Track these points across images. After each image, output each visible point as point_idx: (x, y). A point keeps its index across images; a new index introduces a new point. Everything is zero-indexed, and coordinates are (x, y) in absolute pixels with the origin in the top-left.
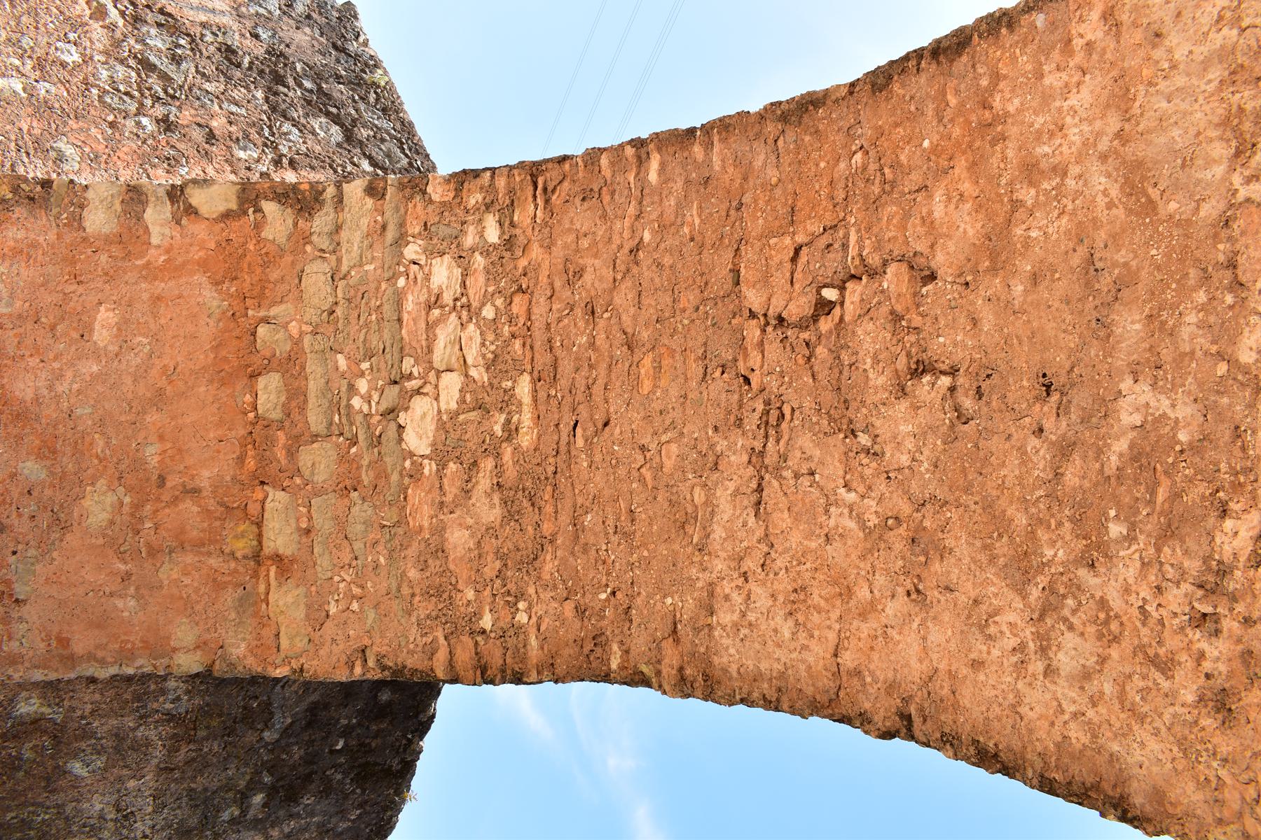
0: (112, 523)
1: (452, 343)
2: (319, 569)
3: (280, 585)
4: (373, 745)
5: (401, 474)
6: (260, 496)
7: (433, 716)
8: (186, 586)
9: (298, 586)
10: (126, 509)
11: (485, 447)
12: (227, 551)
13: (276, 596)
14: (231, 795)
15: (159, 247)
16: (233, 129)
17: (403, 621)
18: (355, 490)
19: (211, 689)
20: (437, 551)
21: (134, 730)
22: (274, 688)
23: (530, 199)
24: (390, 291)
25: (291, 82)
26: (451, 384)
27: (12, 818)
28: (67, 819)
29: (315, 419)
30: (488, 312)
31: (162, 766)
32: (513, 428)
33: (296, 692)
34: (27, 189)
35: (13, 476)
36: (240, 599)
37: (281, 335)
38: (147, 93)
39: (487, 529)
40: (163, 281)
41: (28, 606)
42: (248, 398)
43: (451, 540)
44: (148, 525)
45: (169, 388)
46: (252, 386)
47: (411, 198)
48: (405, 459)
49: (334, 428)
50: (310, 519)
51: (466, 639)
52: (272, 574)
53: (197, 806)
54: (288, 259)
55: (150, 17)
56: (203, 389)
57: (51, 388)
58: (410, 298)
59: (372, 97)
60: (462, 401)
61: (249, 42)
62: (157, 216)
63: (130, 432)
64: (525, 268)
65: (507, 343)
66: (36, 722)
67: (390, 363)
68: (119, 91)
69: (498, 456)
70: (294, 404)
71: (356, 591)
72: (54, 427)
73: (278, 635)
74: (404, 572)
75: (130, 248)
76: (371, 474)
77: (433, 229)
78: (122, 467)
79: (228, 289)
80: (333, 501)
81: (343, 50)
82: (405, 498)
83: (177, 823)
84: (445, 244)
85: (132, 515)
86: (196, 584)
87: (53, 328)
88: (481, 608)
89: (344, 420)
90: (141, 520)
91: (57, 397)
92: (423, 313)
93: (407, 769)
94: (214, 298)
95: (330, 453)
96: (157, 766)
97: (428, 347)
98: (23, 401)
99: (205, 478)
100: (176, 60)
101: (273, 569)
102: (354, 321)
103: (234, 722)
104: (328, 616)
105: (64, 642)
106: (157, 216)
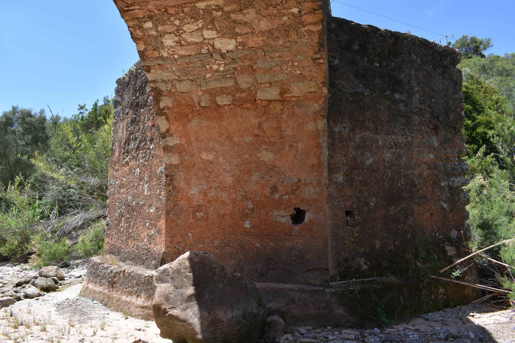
0: (272, 151)
1: (192, 35)
2: (283, 78)
3: (291, 92)
4: (380, 50)
5: (244, 50)
6: (259, 101)
7: (370, 26)
8: (293, 126)
9: (291, 86)
10: (267, 147)
11: (227, 18)
12: (280, 112)
13: (295, 94)
14: (393, 107)
15: (180, 141)
16: (151, 119)
17: (300, 45)
18: (253, 67)
19: (341, 115)
20: (271, 33)
21: (355, 142)
22: (344, 92)
23: (133, 12)
24: (179, 60)
25: (138, 100)
26: (209, 34)
27: (388, 183)
28: (392, 165)
29: (230, 83)
30: (177, 22)
31: (374, 132)
32: (217, 8)
33: (348, 83)
34: (168, 181)
35: (257, 183)
36: (298, 106)
37: (203, 98)
38: (144, 147)
39: (258, 14)
40: (191, 139)
41: (301, 178)
42: (226, 108)
43: (265, 28)
44: (272, 140)
45: (225, 135)
46: (222, 106)
47: (147, 56)
48: (239, 49)
49: (231, 76)
50: (265, 83)
51: (303, 18)
52: (288, 95)
53: (396, 119)
54: (177, 97)
55: (127, 148)
56: (225, 123)
57: (229, 172)
58: (180, 53)
59: (140, 71)
60: (211, 29)
61: (129, 116)
62: (172, 142)
63: (241, 147)
64: (158, 10)
65: (186, 14)
66: (346, 175)
67: (205, 58)
68: (145, 156)
69: (229, 12)
70: (226, 91)
71: (290, 64)
72: (241, 170)
73: (310, 92)
74: (280, 46)
75: (182, 149)
76: (246, 61)
77: (154, 47)
78: (253, 149)
79: (191, 117)
80: (258, 75)
81: (128, 83)
82: (253, 47)
83: (403, 127)
84: (158, 42)
85: (269, 145)
86: (293, 123)
87: (210, 172)
88: (290, 13)
89: (229, 73)
90: (271, 142)
91: (231, 170)
92: (184, 47)
93: (396, 36)
94: (195, 121)
95: (241, 77)
96: (374, 134)
97: (196, 44)
98: (234, 180)
99: (254, 121)
100: (136, 139)
101: (286, 95)
102: (193, 72)
103: (358, 106)
104: (301, 74)
105: (313, 166)
106: (172, 142)
